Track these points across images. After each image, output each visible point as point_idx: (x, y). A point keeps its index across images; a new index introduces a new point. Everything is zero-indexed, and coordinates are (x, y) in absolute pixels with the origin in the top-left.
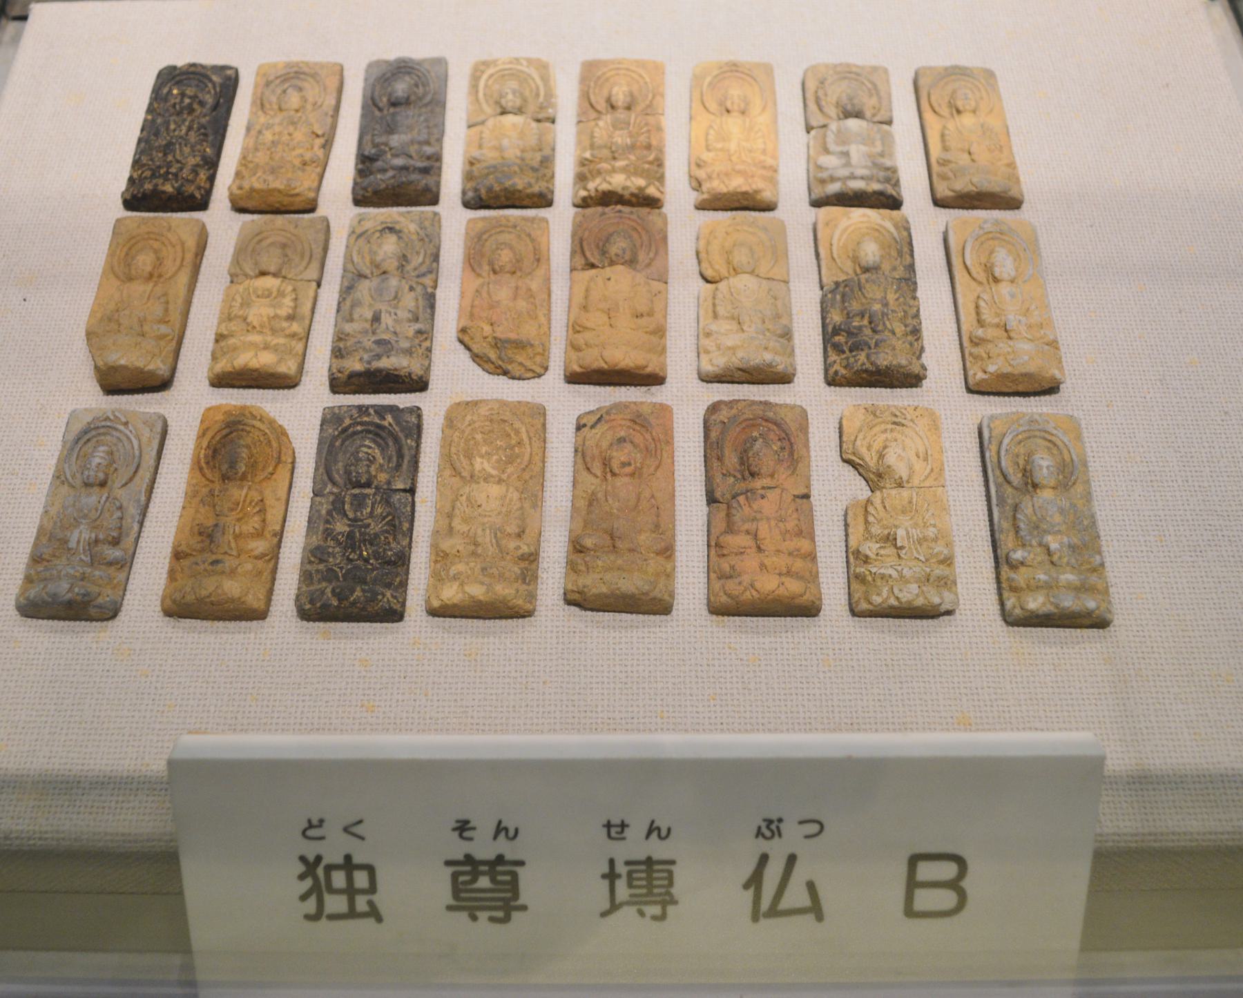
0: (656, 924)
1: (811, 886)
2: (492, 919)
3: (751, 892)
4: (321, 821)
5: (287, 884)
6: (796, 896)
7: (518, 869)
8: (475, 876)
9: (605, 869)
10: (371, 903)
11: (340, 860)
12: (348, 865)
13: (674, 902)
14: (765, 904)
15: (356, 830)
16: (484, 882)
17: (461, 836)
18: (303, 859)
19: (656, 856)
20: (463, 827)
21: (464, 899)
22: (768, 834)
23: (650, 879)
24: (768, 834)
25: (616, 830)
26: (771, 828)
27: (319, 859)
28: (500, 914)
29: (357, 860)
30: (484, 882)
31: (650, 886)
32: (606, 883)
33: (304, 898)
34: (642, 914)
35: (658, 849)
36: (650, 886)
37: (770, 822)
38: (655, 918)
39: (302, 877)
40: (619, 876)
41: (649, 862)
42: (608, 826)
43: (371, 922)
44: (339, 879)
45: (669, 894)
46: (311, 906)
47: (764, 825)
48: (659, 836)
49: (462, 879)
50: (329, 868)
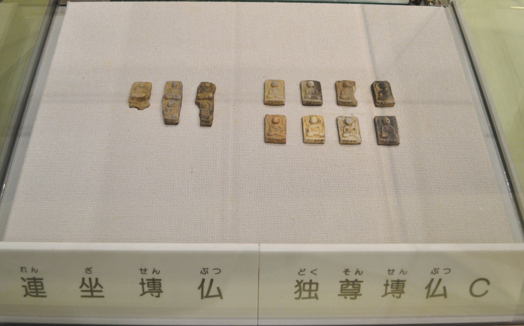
0: (397, 299)
1: (218, 289)
2: (351, 298)
3: (200, 290)
4: (305, 269)
5: (292, 288)
6: (440, 290)
7: (361, 283)
8: (348, 285)
9: (141, 281)
10: (316, 294)
11: (308, 281)
12: (311, 283)
13: (404, 293)
14: (430, 294)
15: (314, 272)
16: (350, 287)
17: (346, 274)
18: (297, 281)
19: (156, 278)
20: (346, 271)
21: (344, 293)
22: (204, 273)
23: (398, 286)
24: (204, 273)
25: (143, 271)
26: (205, 271)
27: (302, 281)
28: (353, 297)
29: (313, 281)
30: (350, 287)
31: (154, 287)
32: (385, 287)
33: (295, 293)
34: (152, 295)
35: (156, 276)
36: (154, 287)
37: (205, 269)
38: (156, 297)
39: (296, 286)
40: (145, 284)
41: (153, 280)
42: (389, 270)
43: (315, 300)
44: (307, 287)
45: (160, 289)
46: (297, 295)
47: (433, 270)
48: (157, 273)
49: (344, 286)
50: (304, 284)
